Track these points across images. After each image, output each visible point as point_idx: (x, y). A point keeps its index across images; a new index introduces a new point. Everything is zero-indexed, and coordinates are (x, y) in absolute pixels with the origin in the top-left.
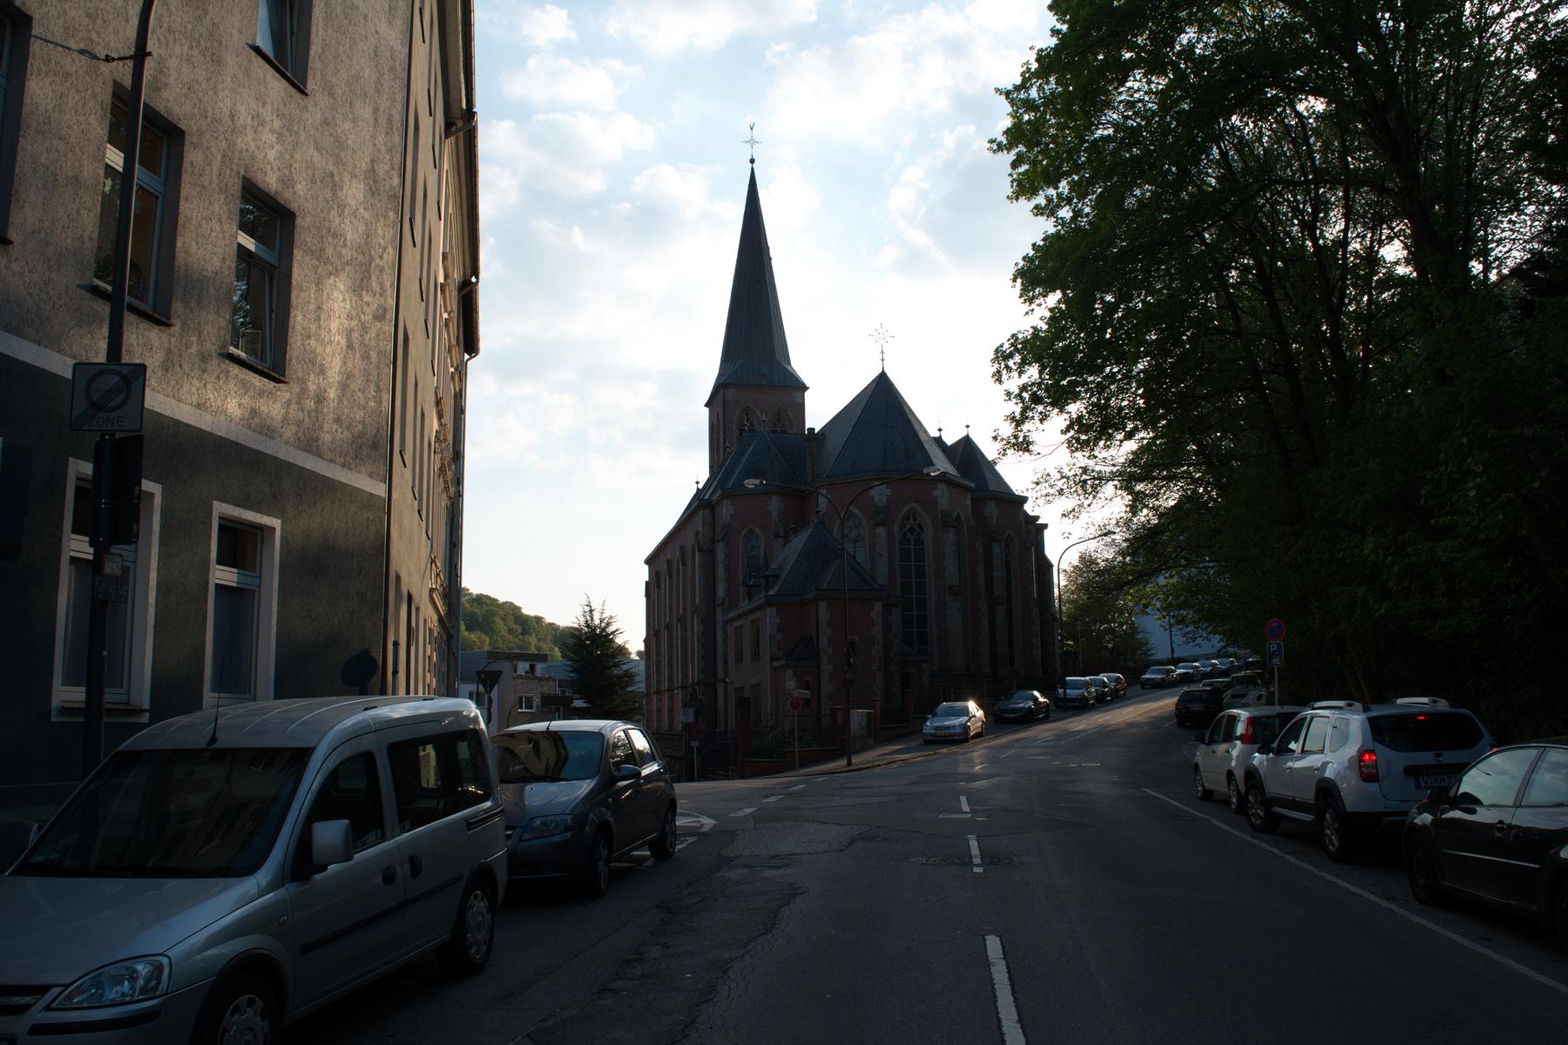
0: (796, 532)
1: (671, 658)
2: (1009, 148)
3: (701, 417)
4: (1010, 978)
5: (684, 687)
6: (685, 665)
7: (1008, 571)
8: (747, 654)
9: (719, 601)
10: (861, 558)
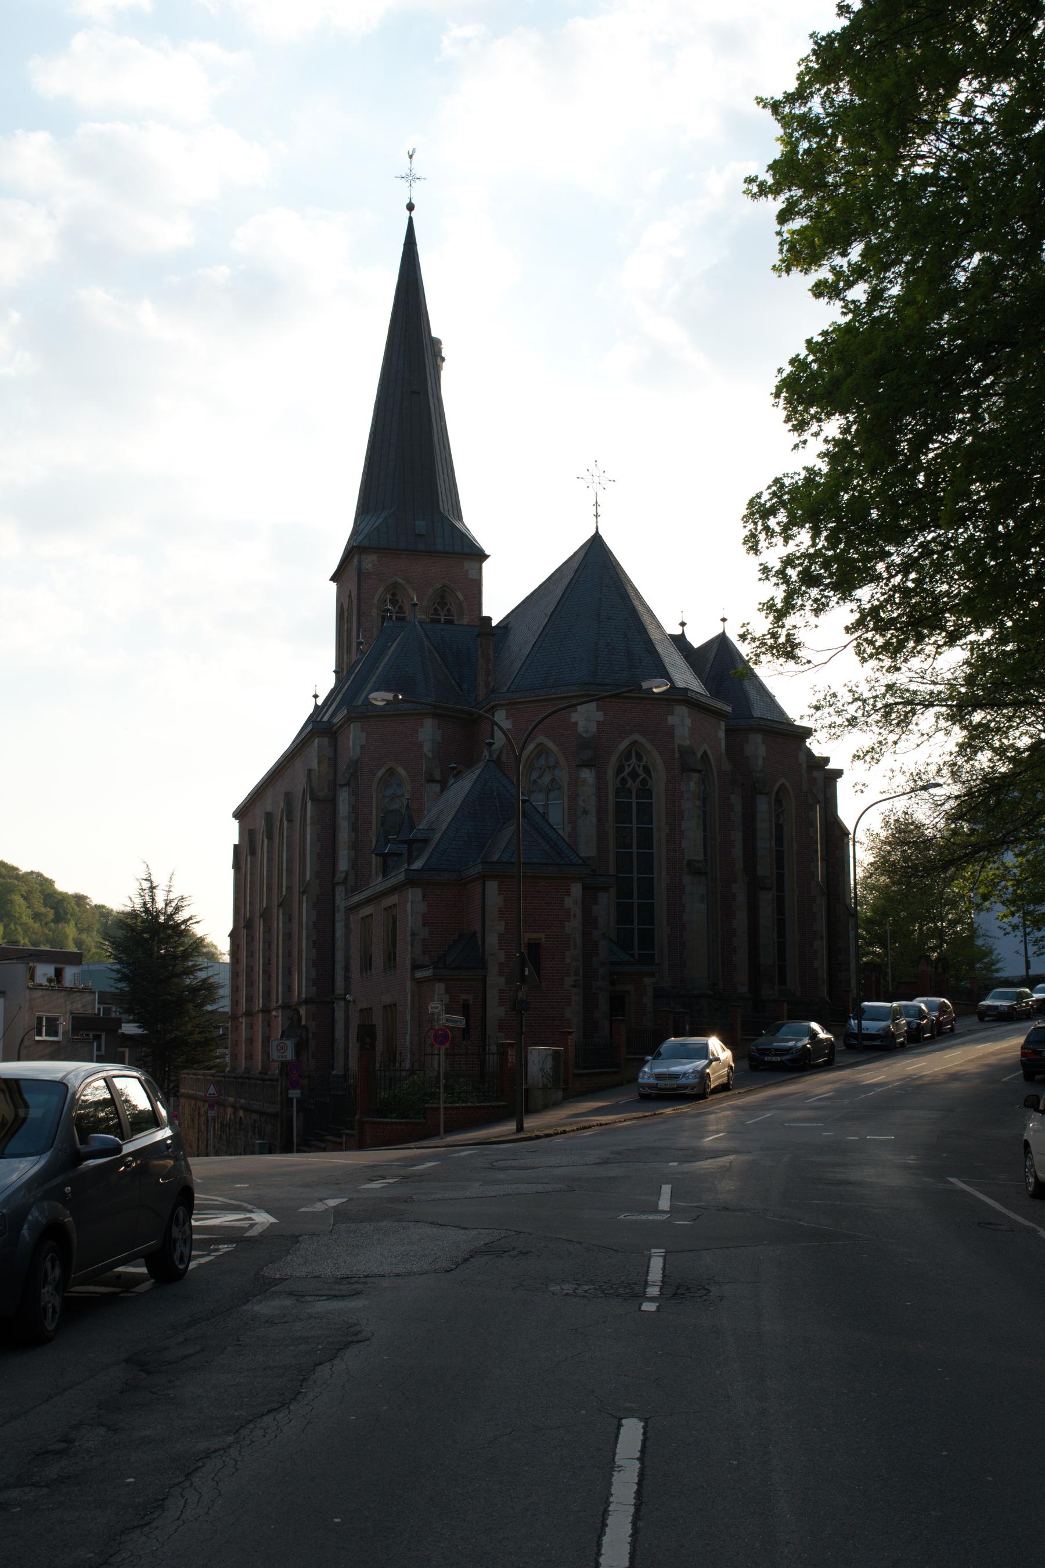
0: (458, 775)
1: (267, 962)
2: (775, 190)
3: (326, 597)
4: (639, 1494)
5: (285, 1007)
6: (288, 972)
7: (779, 840)
8: (378, 959)
9: (340, 877)
10: (556, 817)
